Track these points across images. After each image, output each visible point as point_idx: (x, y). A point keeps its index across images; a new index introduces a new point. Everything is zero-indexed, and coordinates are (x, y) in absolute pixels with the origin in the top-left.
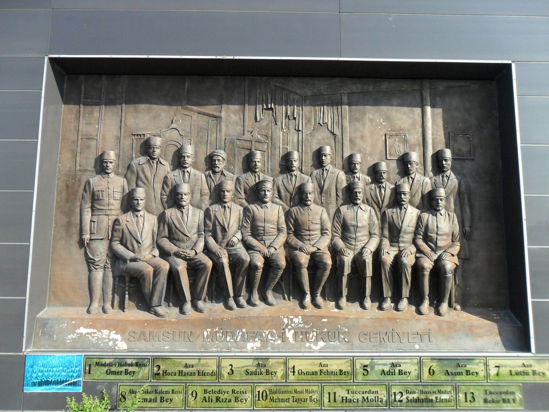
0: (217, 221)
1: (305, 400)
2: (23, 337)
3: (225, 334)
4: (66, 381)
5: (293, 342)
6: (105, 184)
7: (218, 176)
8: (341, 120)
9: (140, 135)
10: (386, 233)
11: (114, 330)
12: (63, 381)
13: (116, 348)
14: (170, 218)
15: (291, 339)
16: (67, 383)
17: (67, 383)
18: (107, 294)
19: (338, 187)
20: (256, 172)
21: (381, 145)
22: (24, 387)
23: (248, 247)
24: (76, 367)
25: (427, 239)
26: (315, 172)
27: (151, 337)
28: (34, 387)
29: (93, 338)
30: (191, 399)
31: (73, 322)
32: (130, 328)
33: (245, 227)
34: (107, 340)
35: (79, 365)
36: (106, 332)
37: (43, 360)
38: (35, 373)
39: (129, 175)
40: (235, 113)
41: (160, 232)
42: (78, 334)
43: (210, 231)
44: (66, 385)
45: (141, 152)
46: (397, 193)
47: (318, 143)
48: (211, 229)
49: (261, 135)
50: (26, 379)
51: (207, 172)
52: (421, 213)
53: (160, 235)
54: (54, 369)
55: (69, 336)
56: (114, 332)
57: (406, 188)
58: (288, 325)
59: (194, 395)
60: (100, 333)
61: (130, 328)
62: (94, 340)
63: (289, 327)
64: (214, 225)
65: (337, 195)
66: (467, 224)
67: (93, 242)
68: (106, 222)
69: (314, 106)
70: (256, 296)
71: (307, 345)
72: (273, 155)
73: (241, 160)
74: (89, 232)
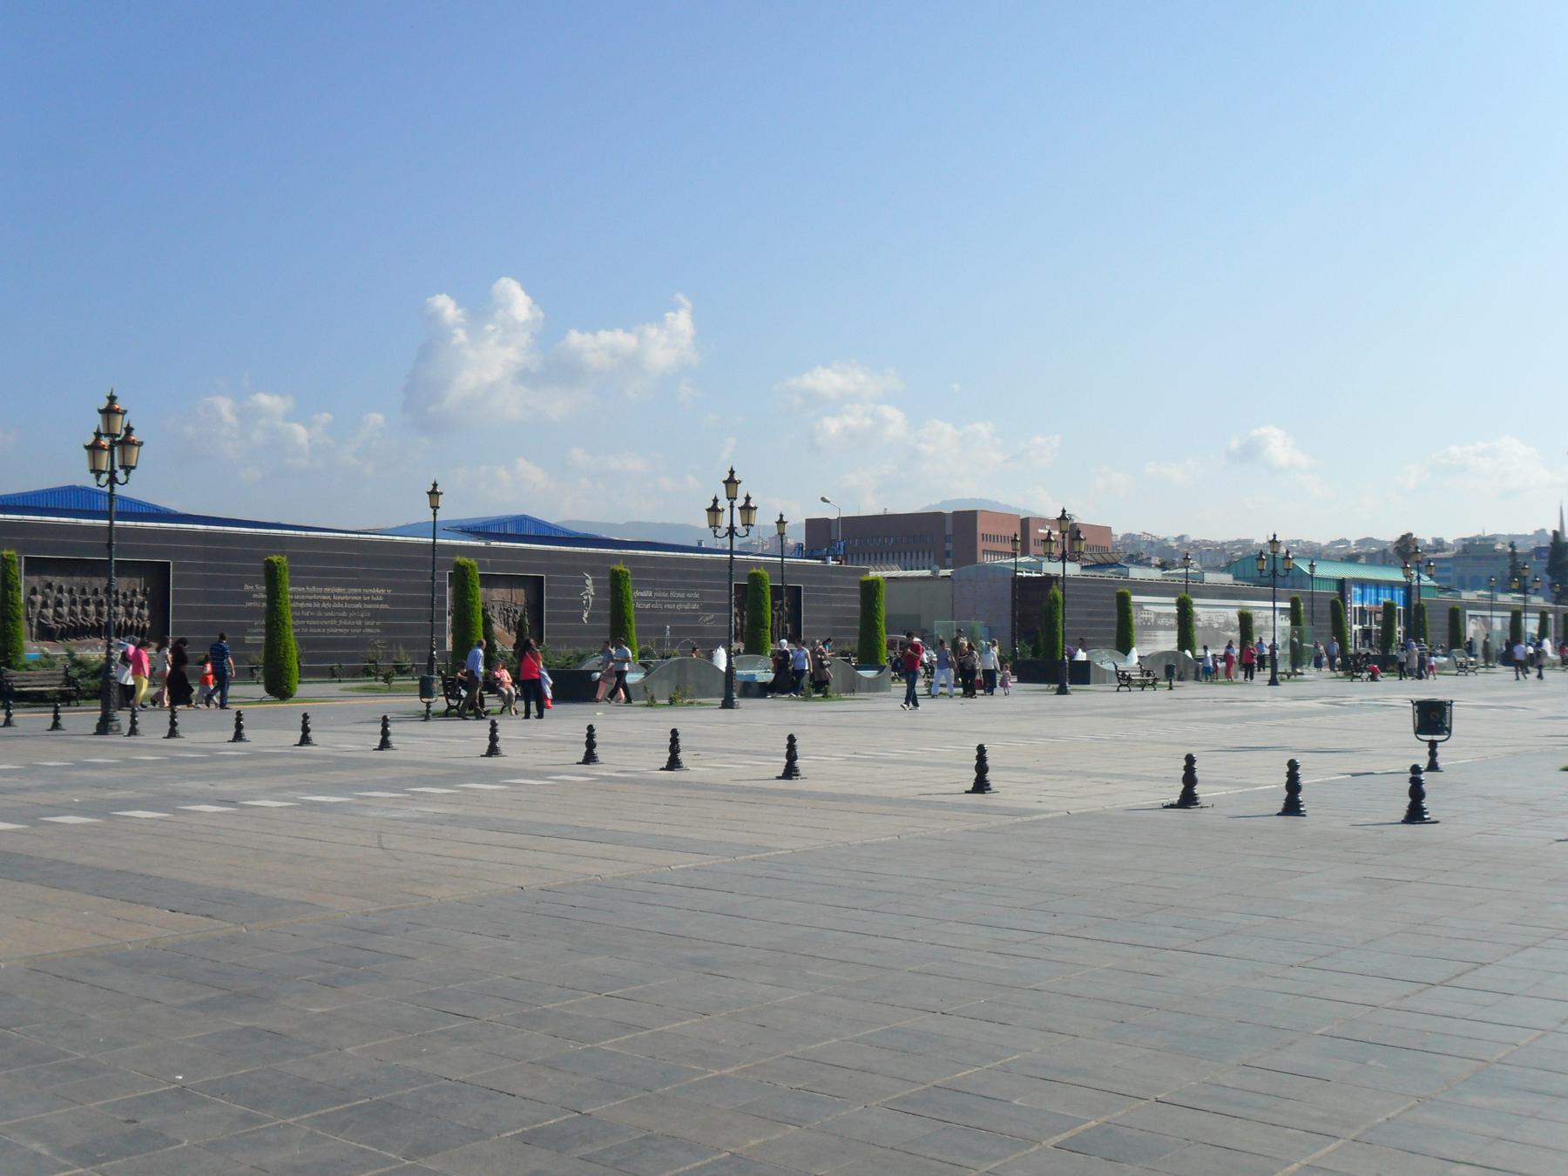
23: (57, 622)
25: (141, 618)
46: (132, 602)
57: (135, 601)
68: (37, 611)
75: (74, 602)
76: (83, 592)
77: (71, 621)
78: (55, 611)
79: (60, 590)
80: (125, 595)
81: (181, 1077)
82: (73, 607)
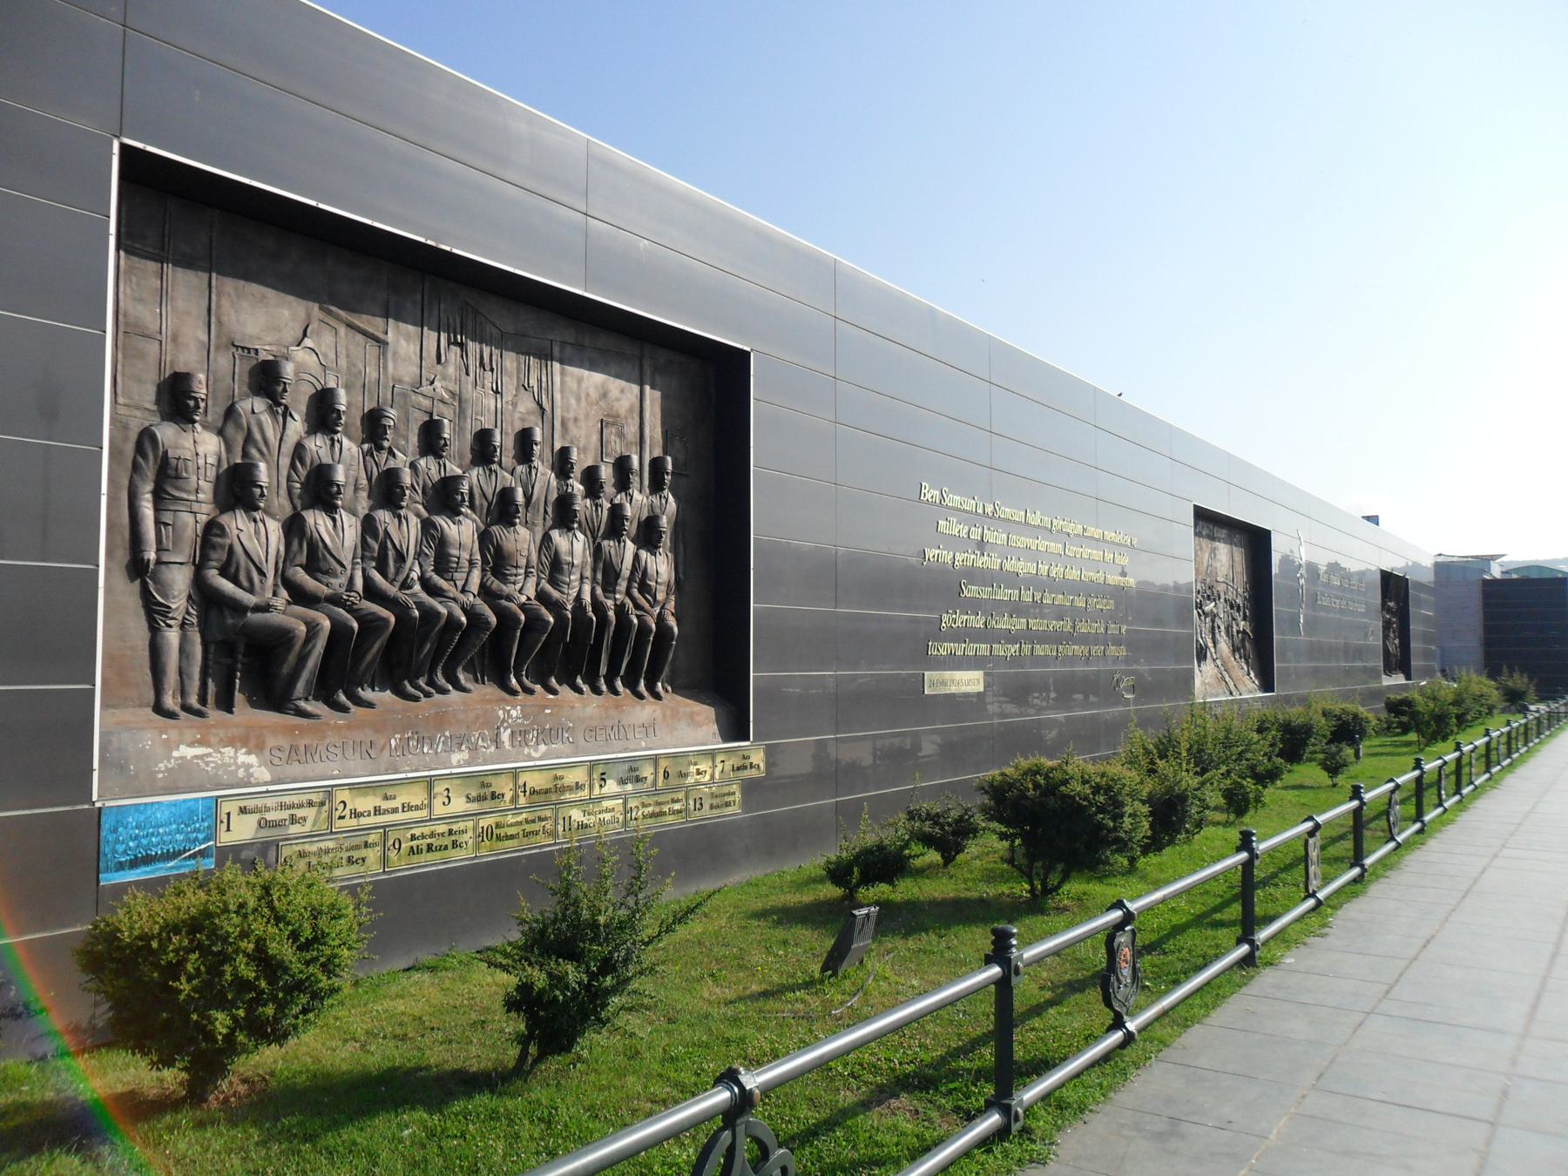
0: (389, 543)
1: (537, 833)
2: (93, 770)
3: (421, 741)
4: (185, 851)
5: (510, 748)
6: (188, 443)
7: (384, 455)
8: (647, 414)
9: (249, 349)
10: (599, 576)
11: (242, 747)
12: (179, 851)
13: (252, 780)
14: (314, 529)
15: (507, 744)
16: (187, 854)
17: (187, 854)
18: (190, 678)
19: (549, 498)
20: (441, 457)
21: (595, 438)
22: (101, 876)
23: (300, 596)
24: (203, 821)
26: (520, 468)
27: (309, 755)
28: (122, 873)
29: (207, 765)
30: (392, 854)
31: (164, 736)
32: (271, 742)
33: (426, 554)
34: (233, 768)
35: (209, 817)
36: (228, 751)
37: (137, 814)
38: (123, 842)
39: (230, 430)
40: (408, 338)
41: (292, 556)
42: (176, 759)
43: (373, 559)
44: (185, 858)
45: (250, 388)
46: (616, 513)
47: (523, 420)
48: (376, 555)
49: (447, 390)
50: (102, 859)
51: (366, 446)
52: (638, 549)
53: (292, 561)
54: (161, 830)
55: (161, 765)
56: (244, 750)
58: (504, 721)
59: (397, 846)
60: (219, 755)
61: (271, 742)
62: (209, 769)
63: (505, 725)
64: (383, 548)
65: (546, 512)
66: (681, 571)
67: (163, 567)
69: (517, 353)
70: (441, 680)
71: (526, 750)
72: (462, 429)
73: (417, 431)
74: (154, 546)
75: (387, 491)
76: (431, 439)
77: (371, 592)
78: (294, 528)
79: (323, 413)
80: (591, 478)
81: (1293, 960)
82: (383, 517)
